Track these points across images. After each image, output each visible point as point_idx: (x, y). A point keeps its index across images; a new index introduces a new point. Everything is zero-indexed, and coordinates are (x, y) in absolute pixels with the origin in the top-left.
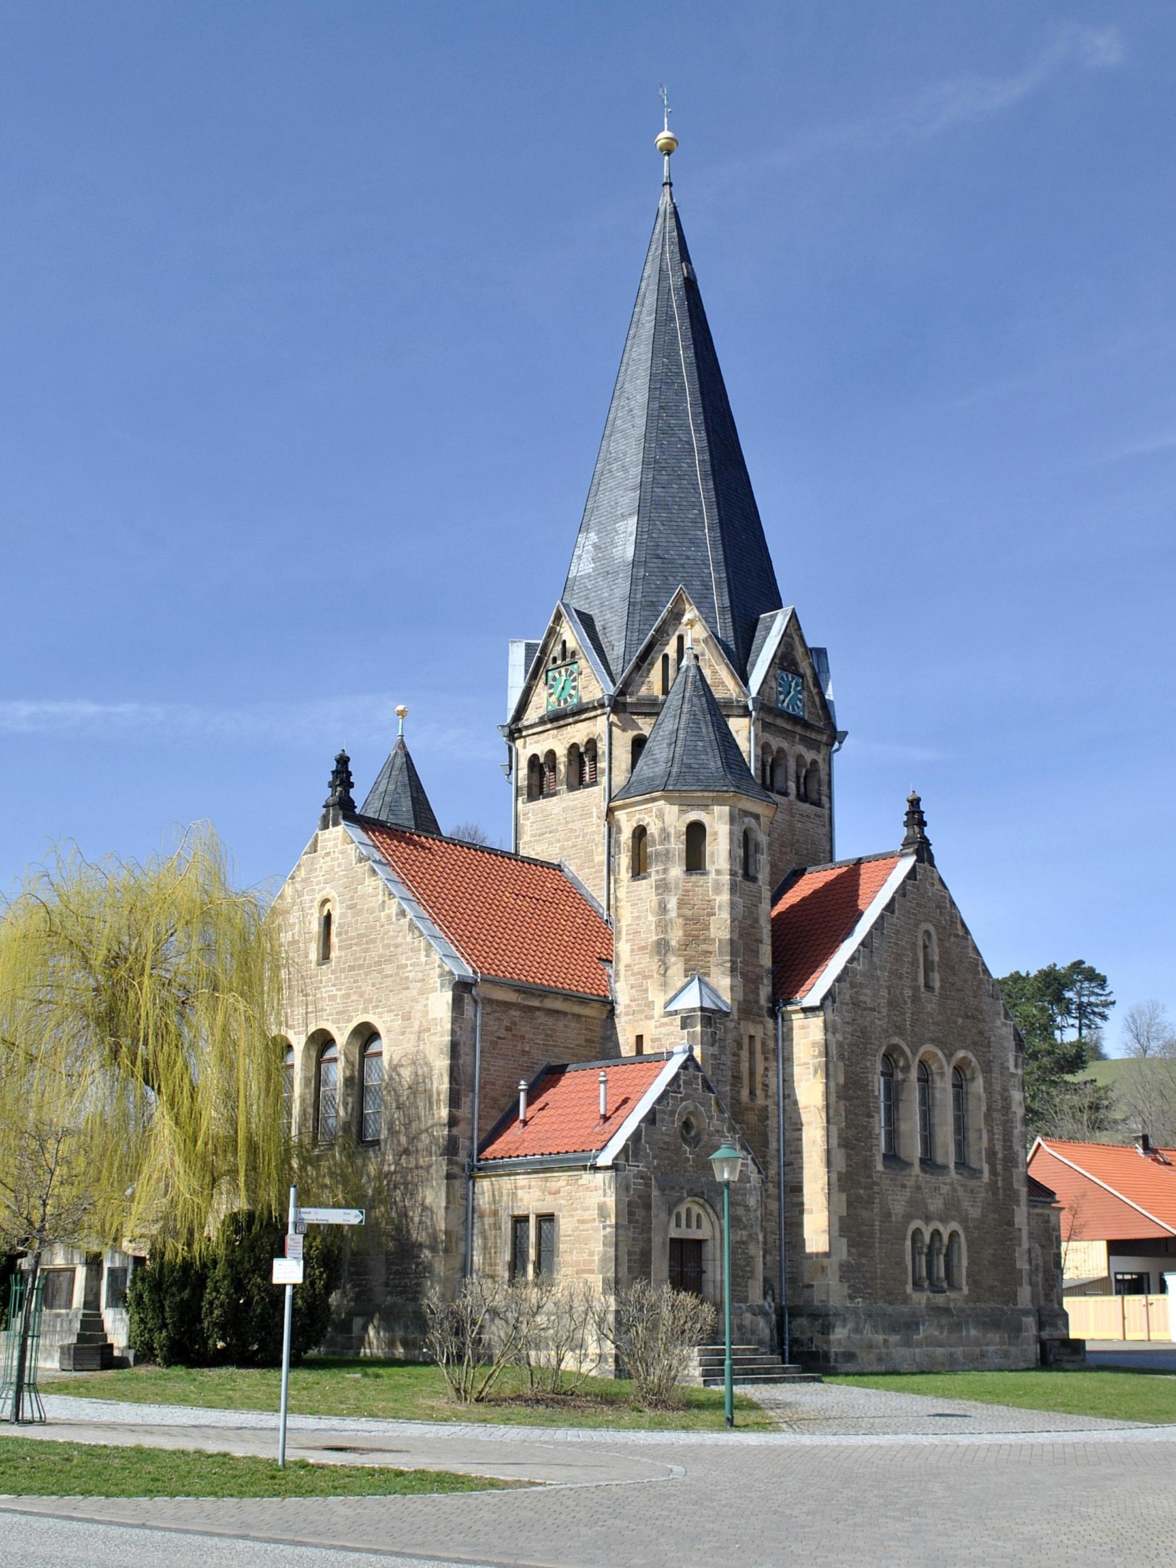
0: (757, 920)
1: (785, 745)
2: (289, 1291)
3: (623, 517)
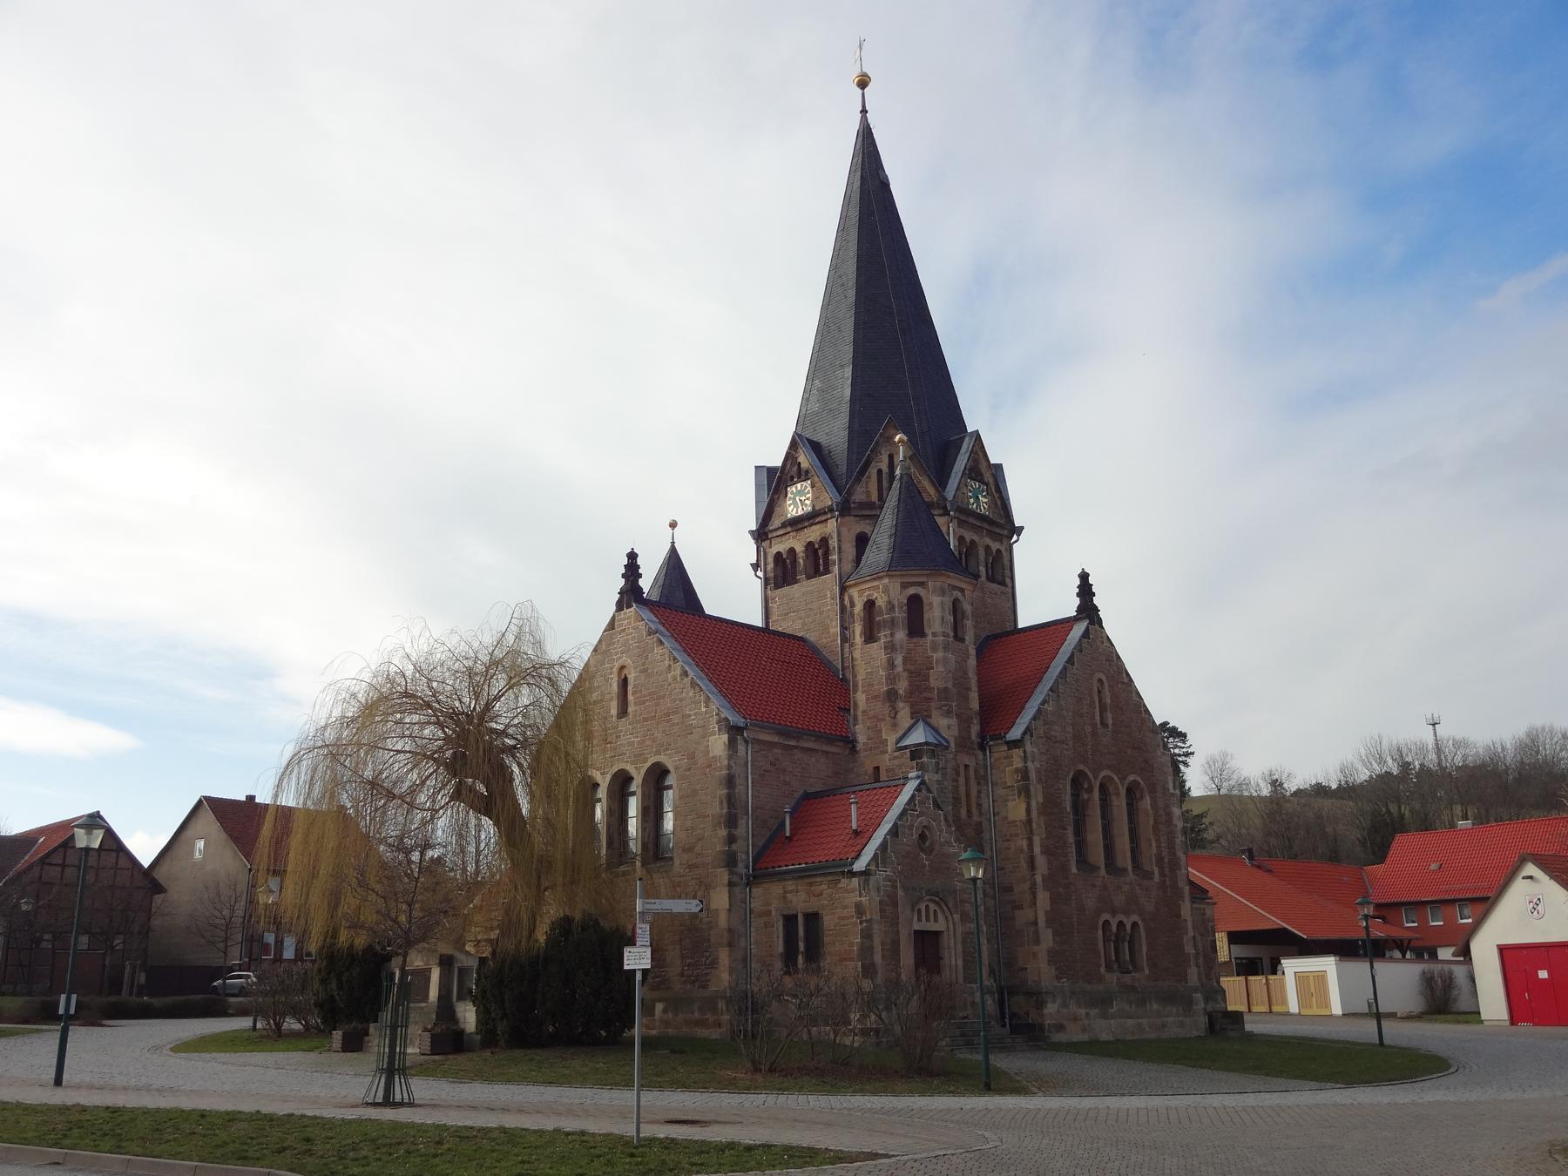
0: (966, 673)
1: (976, 538)
2: (639, 976)
3: (842, 366)
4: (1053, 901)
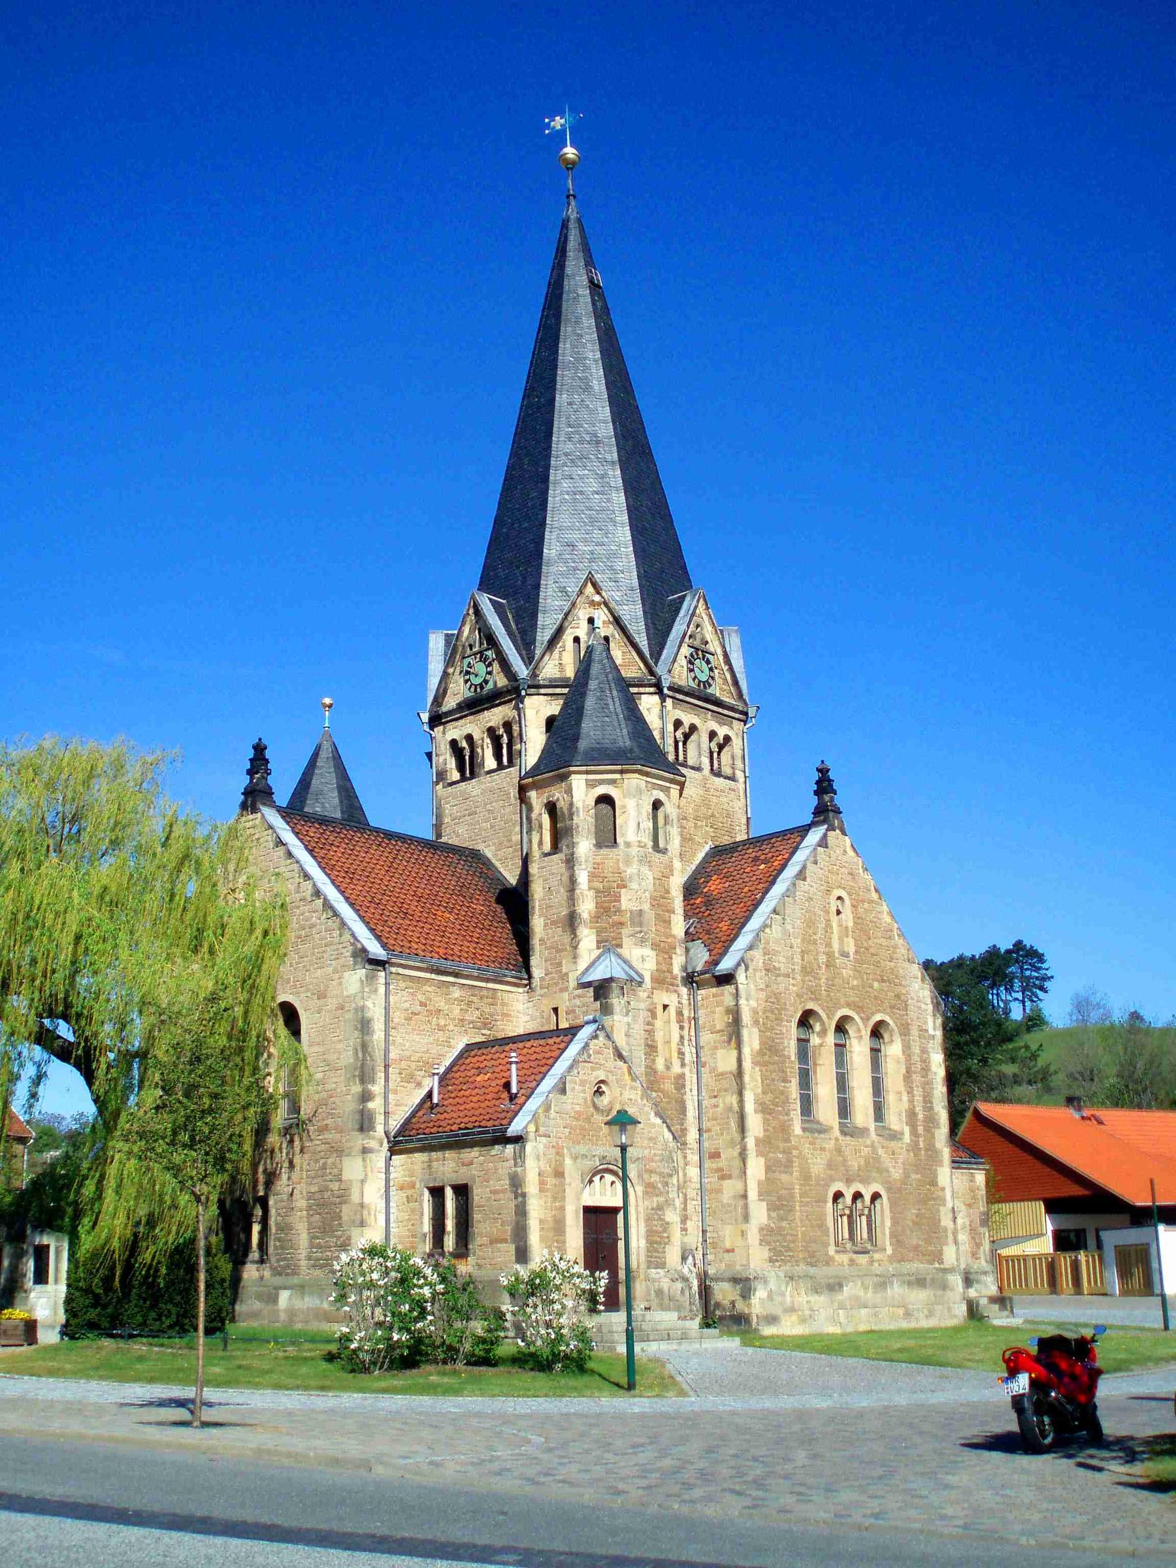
1: (697, 721)
4: (768, 1169)
